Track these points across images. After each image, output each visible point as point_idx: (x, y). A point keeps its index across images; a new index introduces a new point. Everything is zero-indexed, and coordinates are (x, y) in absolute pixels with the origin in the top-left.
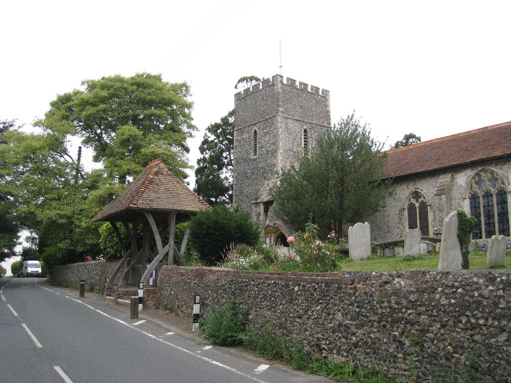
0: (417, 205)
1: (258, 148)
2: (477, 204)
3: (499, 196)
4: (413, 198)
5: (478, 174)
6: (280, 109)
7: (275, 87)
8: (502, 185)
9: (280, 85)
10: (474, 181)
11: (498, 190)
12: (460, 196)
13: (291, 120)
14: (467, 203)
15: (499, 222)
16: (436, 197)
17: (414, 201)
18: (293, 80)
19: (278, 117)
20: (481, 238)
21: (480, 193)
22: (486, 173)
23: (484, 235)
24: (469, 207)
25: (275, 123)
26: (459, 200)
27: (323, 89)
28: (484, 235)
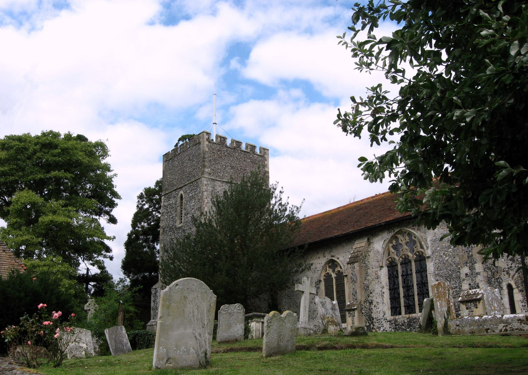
0: (334, 275)
1: (183, 215)
2: (395, 273)
3: (418, 263)
4: (330, 267)
5: (395, 237)
6: (206, 170)
7: (201, 146)
8: (421, 250)
9: (207, 143)
10: (391, 245)
11: (416, 255)
12: (377, 264)
13: (219, 183)
14: (385, 272)
15: (418, 294)
16: (349, 265)
17: (330, 271)
18: (223, 138)
19: (203, 178)
20: (400, 314)
21: (398, 260)
22: (403, 236)
23: (403, 309)
24: (387, 277)
25: (200, 186)
26: (376, 269)
27: (260, 148)
28: (403, 309)
